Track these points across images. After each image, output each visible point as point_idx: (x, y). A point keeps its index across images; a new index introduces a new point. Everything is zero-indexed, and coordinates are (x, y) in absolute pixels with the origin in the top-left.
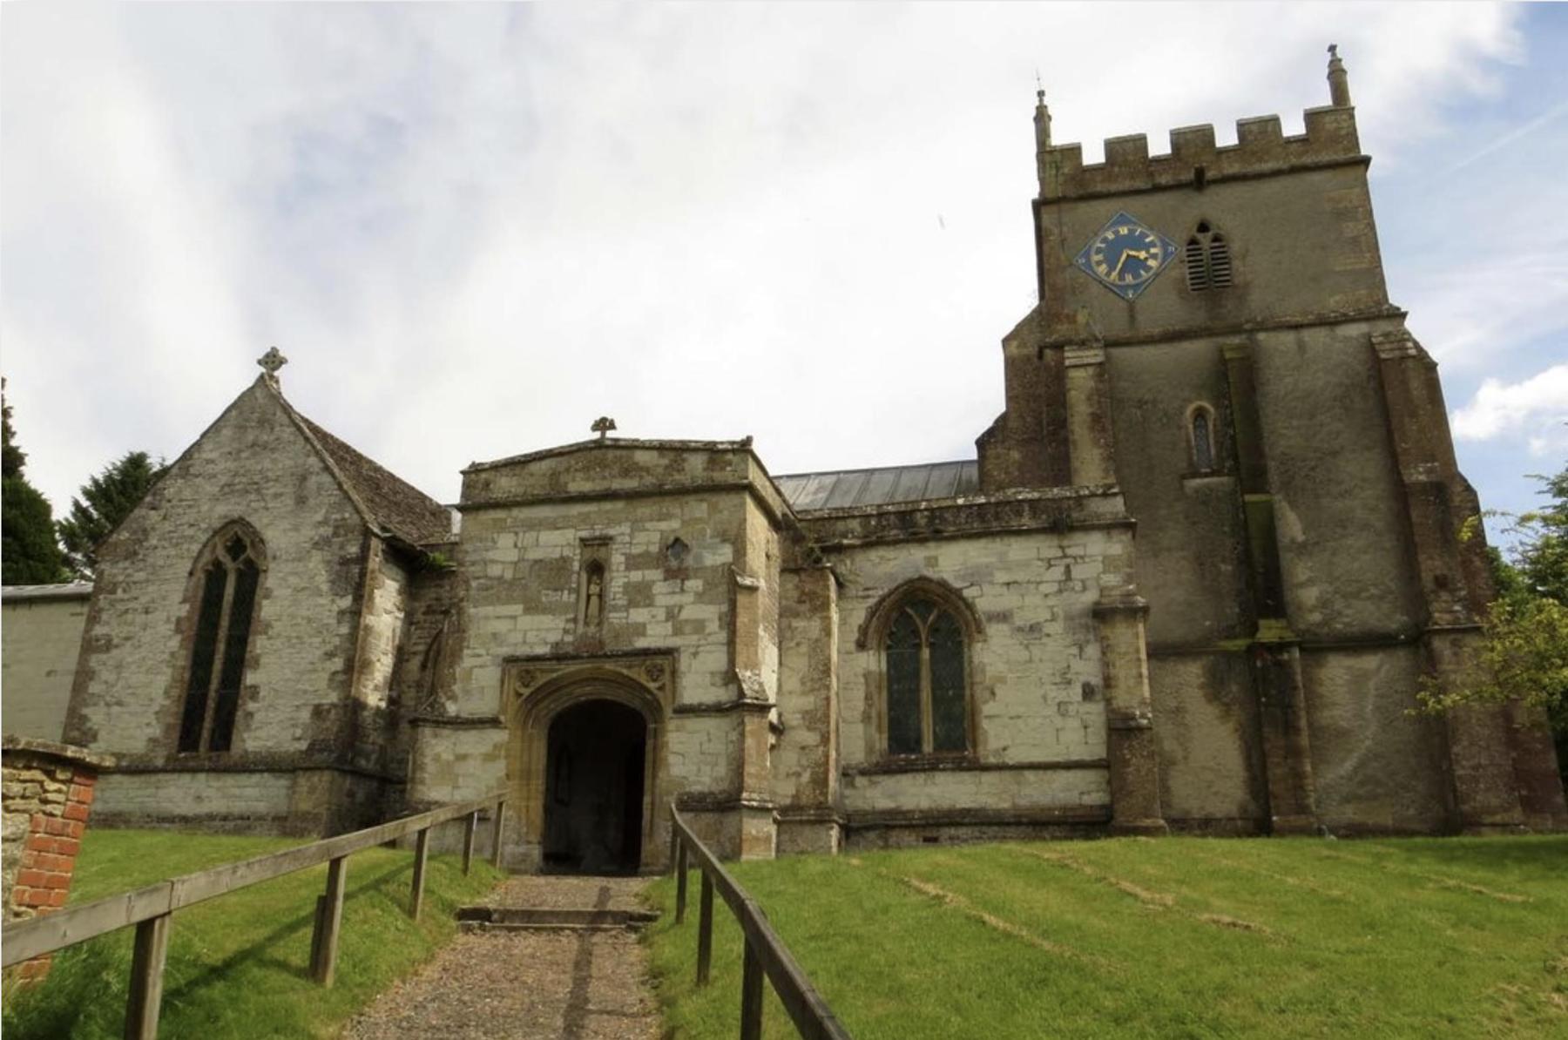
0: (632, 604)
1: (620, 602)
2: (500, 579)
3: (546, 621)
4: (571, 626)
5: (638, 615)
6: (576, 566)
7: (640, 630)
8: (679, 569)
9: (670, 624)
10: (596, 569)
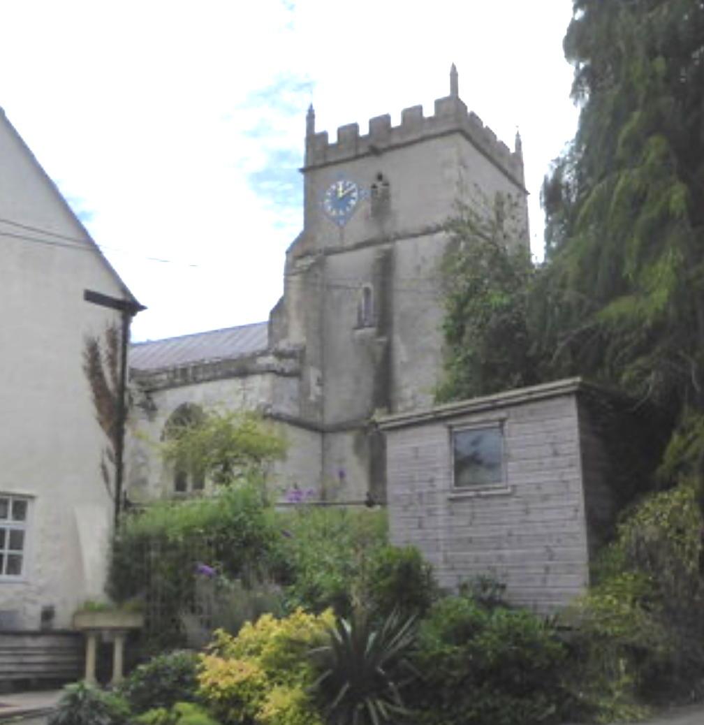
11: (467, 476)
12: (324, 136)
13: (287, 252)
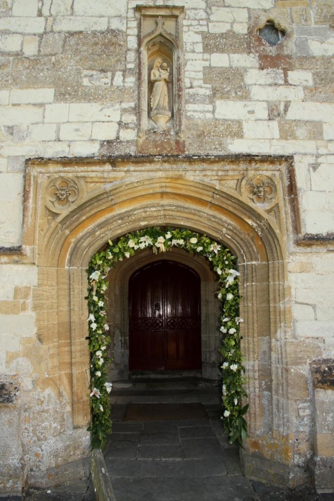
0: (216, 94)
1: (202, 92)
2: (19, 55)
3: (91, 110)
4: (131, 118)
5: (228, 109)
6: (132, 42)
7: (236, 130)
8: (278, 57)
9: (275, 124)
10: (166, 47)
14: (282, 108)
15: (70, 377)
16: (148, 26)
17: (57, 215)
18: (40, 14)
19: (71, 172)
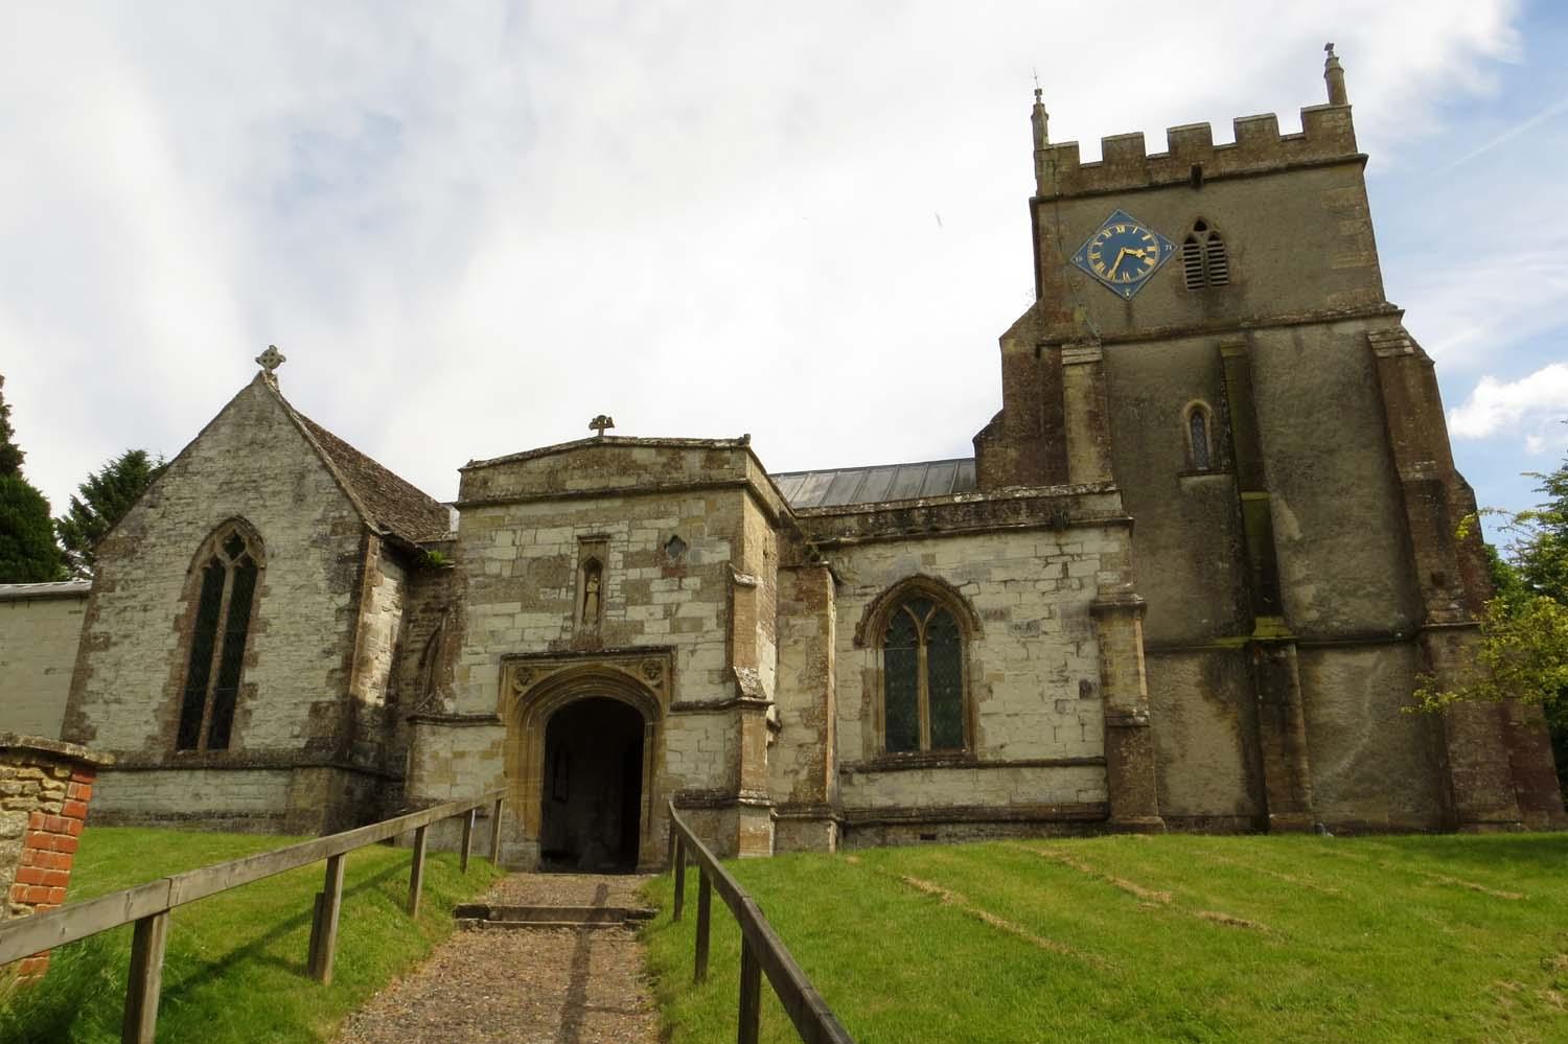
0: (630, 601)
1: (618, 600)
5: (636, 613)
7: (639, 628)
8: (677, 567)
10: (594, 567)
11: (851, 836)
12: (1071, 150)
13: (1003, 340)
14: (674, 609)
15: (525, 805)
16: (586, 551)
17: (519, 693)
18: (514, 544)
19: (529, 664)
